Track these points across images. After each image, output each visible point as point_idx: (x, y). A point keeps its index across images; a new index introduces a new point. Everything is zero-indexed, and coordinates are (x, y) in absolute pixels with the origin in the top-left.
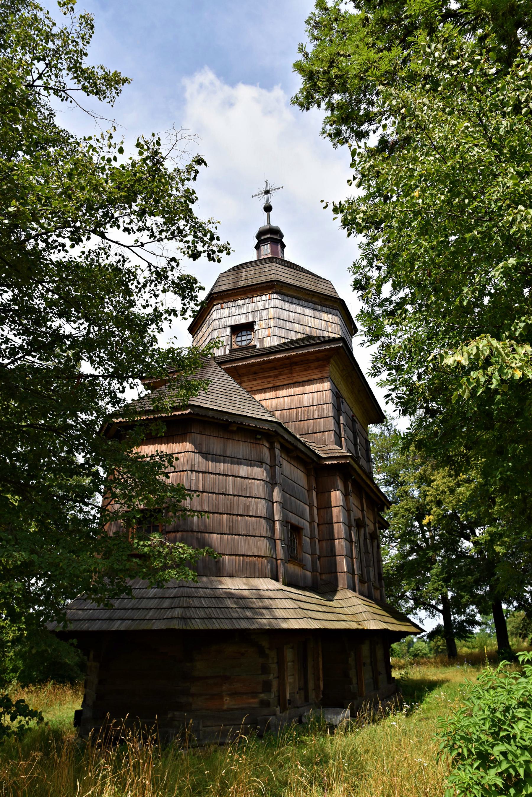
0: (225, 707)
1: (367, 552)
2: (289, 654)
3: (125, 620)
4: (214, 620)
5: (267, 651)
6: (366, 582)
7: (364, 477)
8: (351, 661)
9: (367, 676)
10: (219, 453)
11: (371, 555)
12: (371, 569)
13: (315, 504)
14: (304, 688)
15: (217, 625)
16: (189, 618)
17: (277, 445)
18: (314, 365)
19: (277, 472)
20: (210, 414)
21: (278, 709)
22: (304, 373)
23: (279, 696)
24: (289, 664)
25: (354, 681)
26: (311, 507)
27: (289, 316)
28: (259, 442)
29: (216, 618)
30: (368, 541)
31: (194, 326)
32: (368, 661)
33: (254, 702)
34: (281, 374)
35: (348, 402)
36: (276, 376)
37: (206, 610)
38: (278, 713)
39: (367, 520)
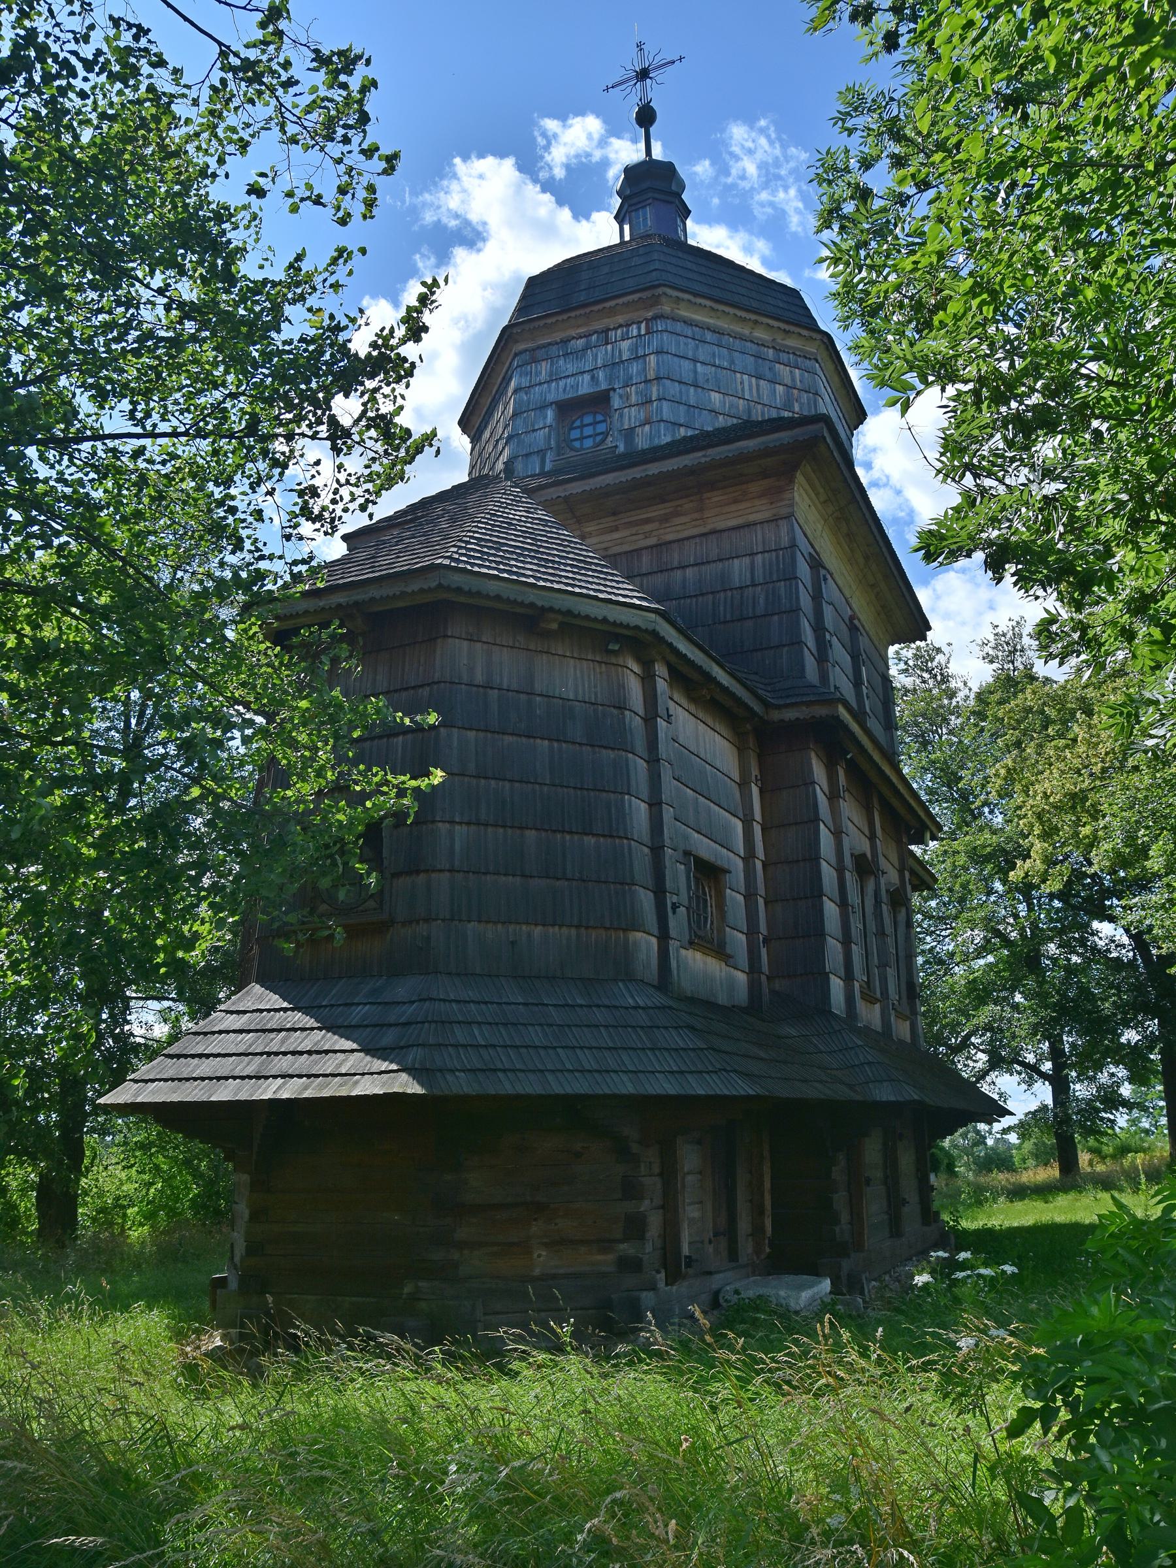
0: (537, 1272)
1: (881, 933)
2: (690, 1158)
3: (291, 1076)
4: (500, 1074)
5: (635, 1148)
6: (876, 1000)
7: (877, 757)
8: (838, 1173)
9: (874, 1207)
10: (514, 686)
11: (890, 941)
12: (891, 972)
13: (758, 816)
14: (729, 1233)
15: (507, 1086)
16: (440, 1071)
17: (660, 669)
18: (754, 488)
19: (661, 735)
20: (493, 587)
21: (663, 1275)
22: (733, 507)
23: (664, 1248)
24: (689, 1178)
25: (845, 1217)
26: (747, 823)
27: (695, 372)
28: (614, 661)
29: (504, 1071)
30: (884, 907)
31: (472, 413)
32: (878, 1174)
33: (605, 1261)
34: (676, 514)
35: (840, 582)
36: (665, 519)
37: (483, 1051)
38: (661, 1285)
39: (882, 860)
